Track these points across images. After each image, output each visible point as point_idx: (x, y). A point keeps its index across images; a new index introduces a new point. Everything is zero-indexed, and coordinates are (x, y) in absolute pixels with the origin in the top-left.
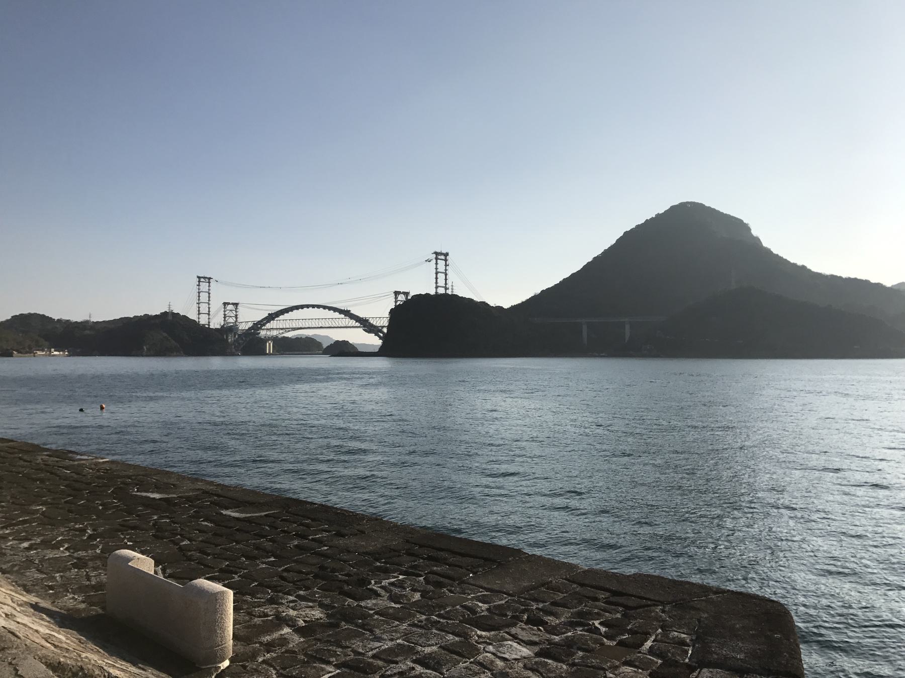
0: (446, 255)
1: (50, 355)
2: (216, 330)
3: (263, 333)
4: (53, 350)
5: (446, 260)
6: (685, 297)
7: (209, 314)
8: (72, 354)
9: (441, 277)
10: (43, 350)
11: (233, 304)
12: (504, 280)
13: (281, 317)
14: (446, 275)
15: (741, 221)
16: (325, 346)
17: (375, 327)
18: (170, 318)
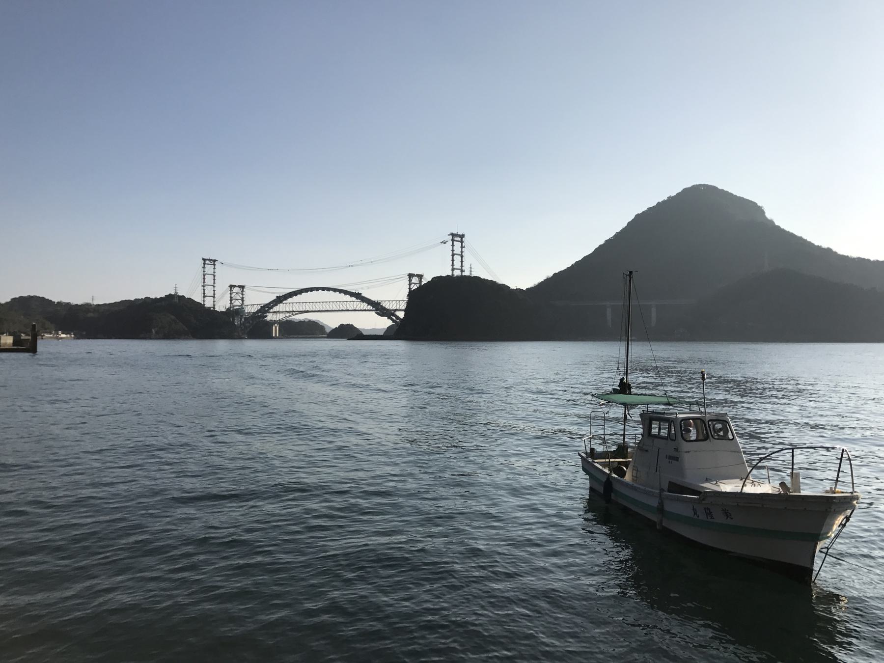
0: (462, 236)
2: (222, 312)
4: (60, 332)
5: (462, 242)
6: (699, 278)
7: (214, 297)
8: (78, 337)
9: (457, 259)
10: (51, 333)
11: (239, 287)
12: (520, 265)
13: (290, 300)
14: (462, 257)
15: (755, 204)
16: (328, 331)
17: (388, 310)
18: (176, 300)
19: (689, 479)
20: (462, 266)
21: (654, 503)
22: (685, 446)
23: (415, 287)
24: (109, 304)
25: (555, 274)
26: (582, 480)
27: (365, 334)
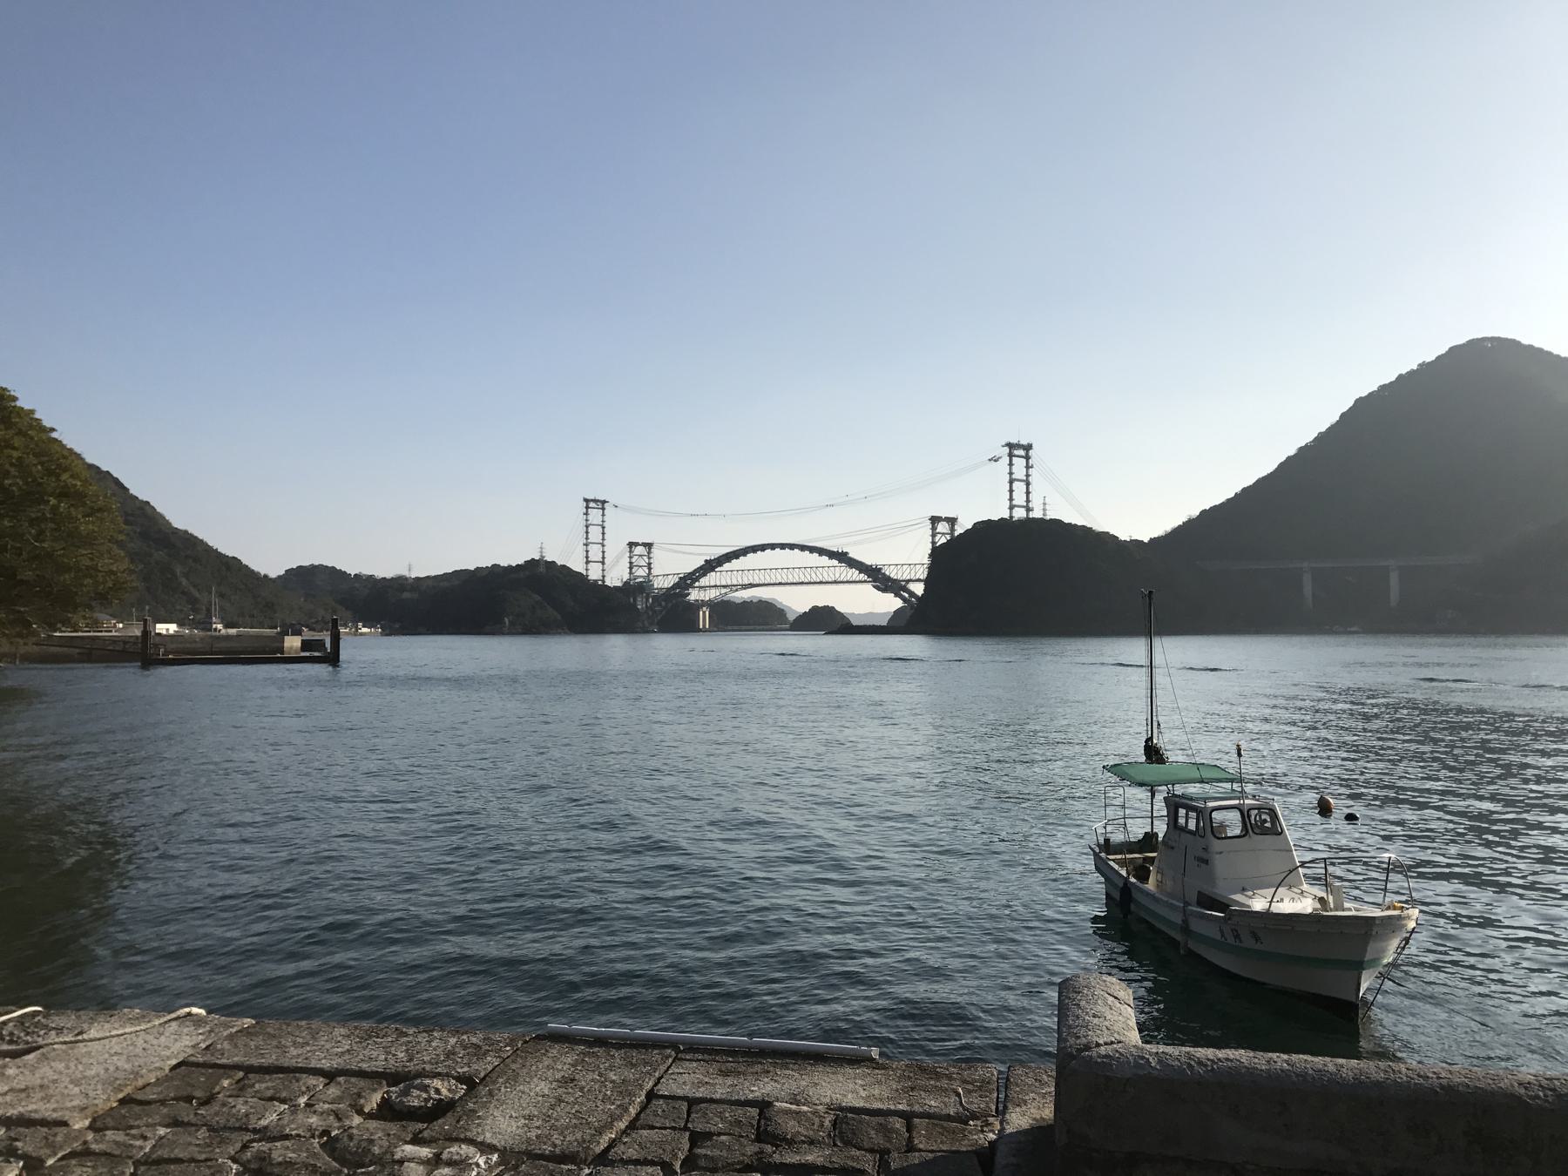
0: (1028, 448)
1: (356, 634)
3: (694, 595)
5: (1027, 458)
8: (389, 631)
9: (1019, 488)
11: (644, 545)
12: (1139, 487)
13: (727, 566)
14: (1028, 484)
16: (791, 617)
19: (1220, 891)
20: (1028, 501)
21: (1177, 918)
22: (1217, 845)
23: (943, 540)
24: (436, 577)
25: (1343, 415)
26: (1095, 884)
27: (855, 622)
